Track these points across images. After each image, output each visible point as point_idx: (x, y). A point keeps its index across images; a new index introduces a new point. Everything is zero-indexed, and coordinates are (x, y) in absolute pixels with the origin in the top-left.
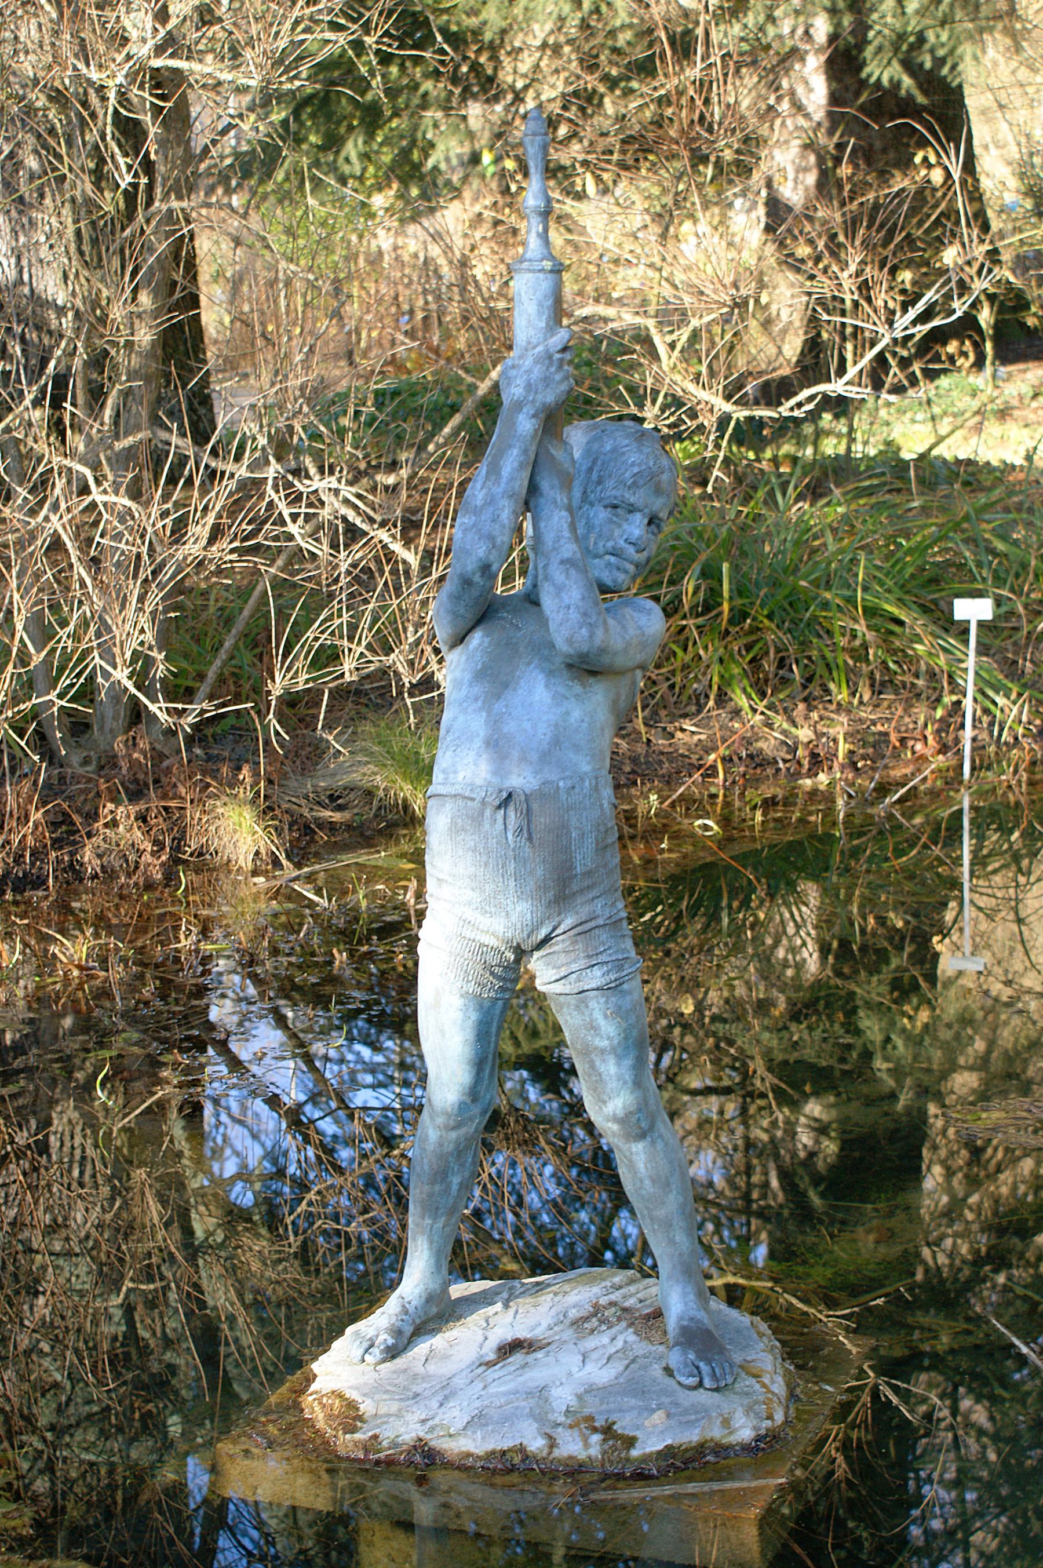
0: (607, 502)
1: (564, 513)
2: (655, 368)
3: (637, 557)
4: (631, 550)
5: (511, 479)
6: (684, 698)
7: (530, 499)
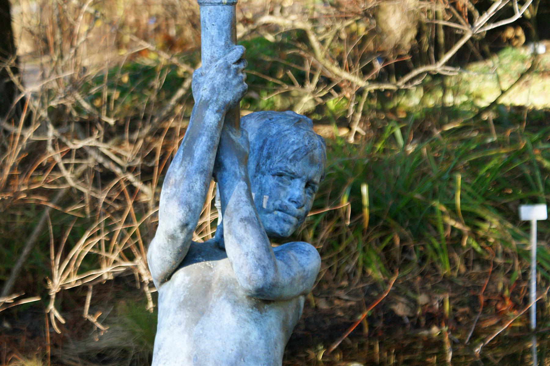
0: (274, 172)
1: (242, 183)
2: (312, 59)
3: (297, 211)
4: (293, 207)
5: (202, 159)
6: (340, 276)
7: (217, 172)
